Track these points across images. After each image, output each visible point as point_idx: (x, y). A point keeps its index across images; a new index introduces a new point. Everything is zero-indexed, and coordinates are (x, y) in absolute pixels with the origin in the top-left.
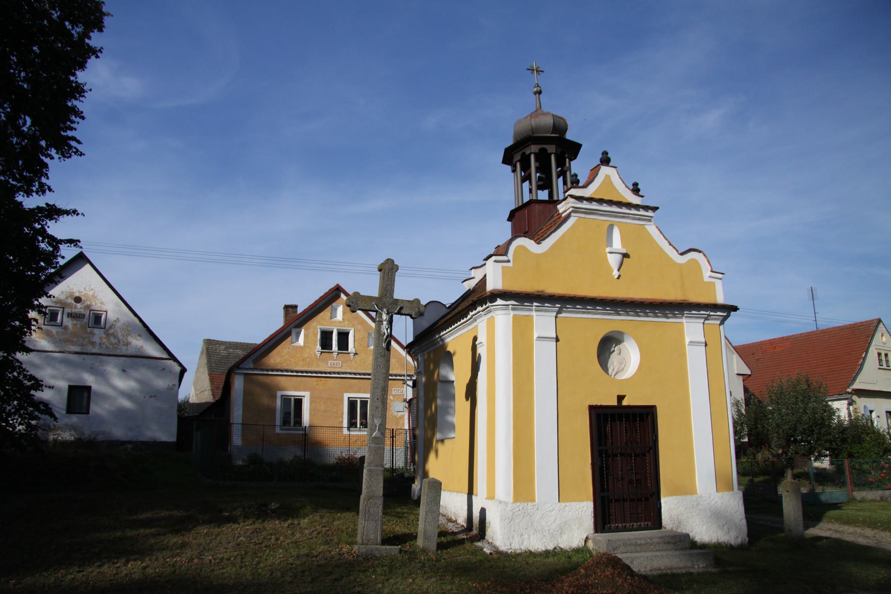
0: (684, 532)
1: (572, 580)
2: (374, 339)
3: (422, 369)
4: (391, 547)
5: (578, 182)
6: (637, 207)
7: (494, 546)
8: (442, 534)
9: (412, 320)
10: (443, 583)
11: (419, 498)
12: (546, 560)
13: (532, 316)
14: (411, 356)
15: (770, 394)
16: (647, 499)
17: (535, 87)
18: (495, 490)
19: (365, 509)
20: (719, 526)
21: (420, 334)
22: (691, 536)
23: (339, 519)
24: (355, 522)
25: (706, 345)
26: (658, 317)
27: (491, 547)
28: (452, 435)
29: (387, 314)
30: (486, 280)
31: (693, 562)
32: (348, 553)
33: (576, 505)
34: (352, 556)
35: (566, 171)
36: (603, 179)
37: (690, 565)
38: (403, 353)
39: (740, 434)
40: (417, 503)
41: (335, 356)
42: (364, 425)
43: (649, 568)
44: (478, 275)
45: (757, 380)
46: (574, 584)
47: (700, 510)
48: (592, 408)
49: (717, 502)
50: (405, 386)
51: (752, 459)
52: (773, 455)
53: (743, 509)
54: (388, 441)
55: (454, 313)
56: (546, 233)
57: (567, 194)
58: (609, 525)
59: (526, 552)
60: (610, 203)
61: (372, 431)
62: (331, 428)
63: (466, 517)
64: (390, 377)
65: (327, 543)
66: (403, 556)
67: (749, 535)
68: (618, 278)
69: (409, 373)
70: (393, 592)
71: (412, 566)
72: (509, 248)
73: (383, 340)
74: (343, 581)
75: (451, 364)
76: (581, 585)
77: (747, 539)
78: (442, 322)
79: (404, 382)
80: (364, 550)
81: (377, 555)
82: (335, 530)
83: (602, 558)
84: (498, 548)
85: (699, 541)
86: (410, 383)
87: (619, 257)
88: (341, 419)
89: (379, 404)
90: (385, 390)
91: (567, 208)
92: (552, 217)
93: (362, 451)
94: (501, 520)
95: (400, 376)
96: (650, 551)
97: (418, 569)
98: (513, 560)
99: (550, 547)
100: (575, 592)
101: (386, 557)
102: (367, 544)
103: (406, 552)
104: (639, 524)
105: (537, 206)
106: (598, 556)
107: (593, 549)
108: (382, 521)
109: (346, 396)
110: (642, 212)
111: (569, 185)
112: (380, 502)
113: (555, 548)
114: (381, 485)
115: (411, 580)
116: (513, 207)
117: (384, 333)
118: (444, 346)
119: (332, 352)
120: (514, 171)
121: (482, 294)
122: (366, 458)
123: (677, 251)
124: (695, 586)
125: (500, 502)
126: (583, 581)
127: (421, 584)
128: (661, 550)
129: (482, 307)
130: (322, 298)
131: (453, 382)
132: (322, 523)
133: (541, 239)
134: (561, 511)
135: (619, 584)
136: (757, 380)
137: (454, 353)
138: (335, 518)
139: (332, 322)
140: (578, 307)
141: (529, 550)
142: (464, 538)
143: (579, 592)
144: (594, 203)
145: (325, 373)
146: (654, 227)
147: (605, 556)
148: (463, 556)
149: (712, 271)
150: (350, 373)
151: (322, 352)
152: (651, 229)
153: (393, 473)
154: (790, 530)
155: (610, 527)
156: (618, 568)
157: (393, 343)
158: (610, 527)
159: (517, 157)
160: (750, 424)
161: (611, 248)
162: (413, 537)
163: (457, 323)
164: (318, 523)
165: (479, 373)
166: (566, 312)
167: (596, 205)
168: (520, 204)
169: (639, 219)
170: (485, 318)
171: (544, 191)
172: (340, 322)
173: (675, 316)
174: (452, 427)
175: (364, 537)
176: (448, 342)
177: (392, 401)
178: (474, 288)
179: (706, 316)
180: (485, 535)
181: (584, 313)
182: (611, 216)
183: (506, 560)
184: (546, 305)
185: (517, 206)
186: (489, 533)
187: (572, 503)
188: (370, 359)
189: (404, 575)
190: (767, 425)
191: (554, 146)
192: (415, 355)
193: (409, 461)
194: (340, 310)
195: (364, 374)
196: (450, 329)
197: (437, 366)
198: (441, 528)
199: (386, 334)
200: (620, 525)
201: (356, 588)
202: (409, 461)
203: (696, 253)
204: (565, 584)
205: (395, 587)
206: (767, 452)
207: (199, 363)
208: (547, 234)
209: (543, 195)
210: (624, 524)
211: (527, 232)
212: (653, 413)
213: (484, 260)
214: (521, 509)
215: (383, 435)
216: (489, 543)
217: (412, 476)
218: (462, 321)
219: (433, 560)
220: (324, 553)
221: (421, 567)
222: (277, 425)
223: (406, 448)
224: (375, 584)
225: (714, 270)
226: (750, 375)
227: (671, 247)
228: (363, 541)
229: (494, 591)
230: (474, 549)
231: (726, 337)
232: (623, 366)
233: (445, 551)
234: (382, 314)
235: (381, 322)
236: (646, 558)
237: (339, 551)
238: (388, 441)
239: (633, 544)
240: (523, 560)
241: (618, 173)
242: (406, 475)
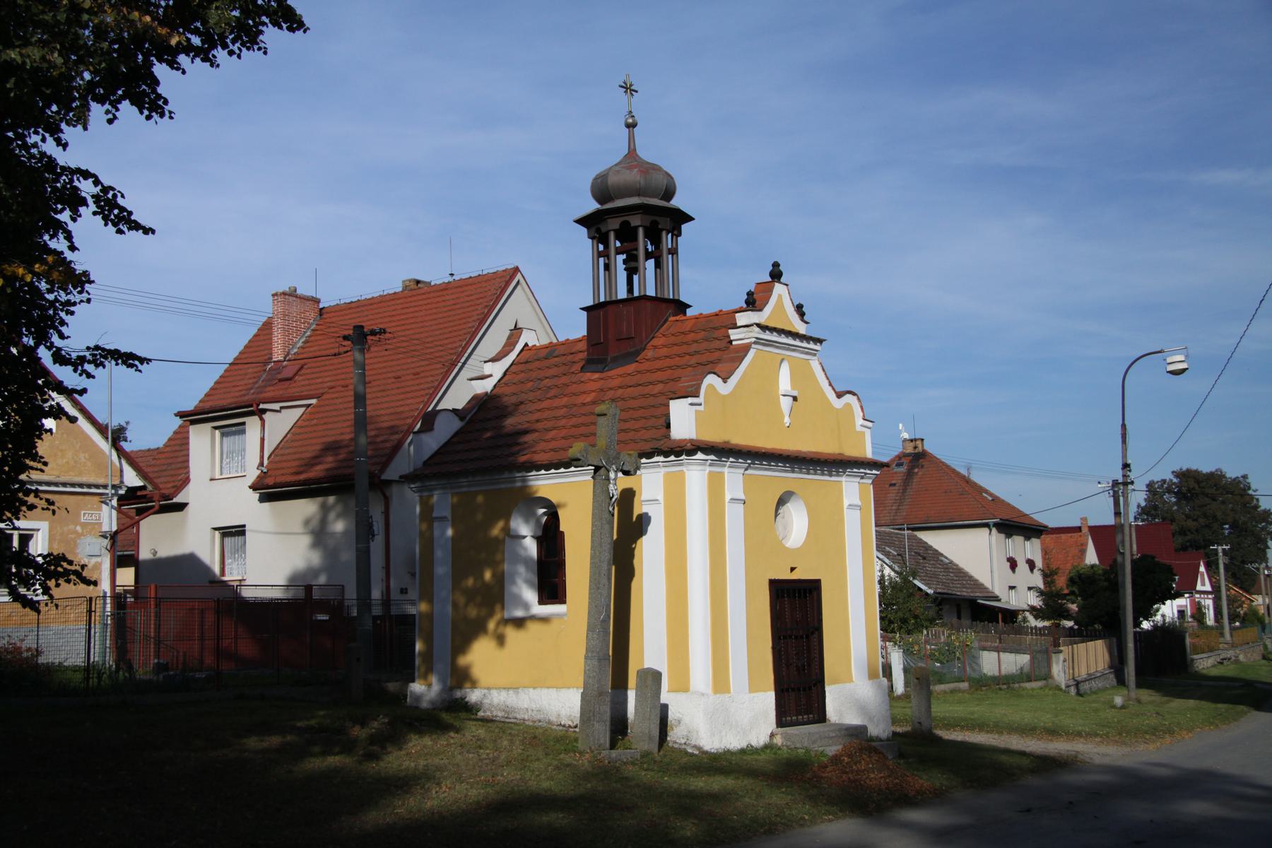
13: (722, 473)
33: (761, 695)
48: (818, 581)
95: (97, 486)
146: (817, 362)
154: (920, 723)
173: (838, 475)
225: (866, 418)
227: (830, 388)
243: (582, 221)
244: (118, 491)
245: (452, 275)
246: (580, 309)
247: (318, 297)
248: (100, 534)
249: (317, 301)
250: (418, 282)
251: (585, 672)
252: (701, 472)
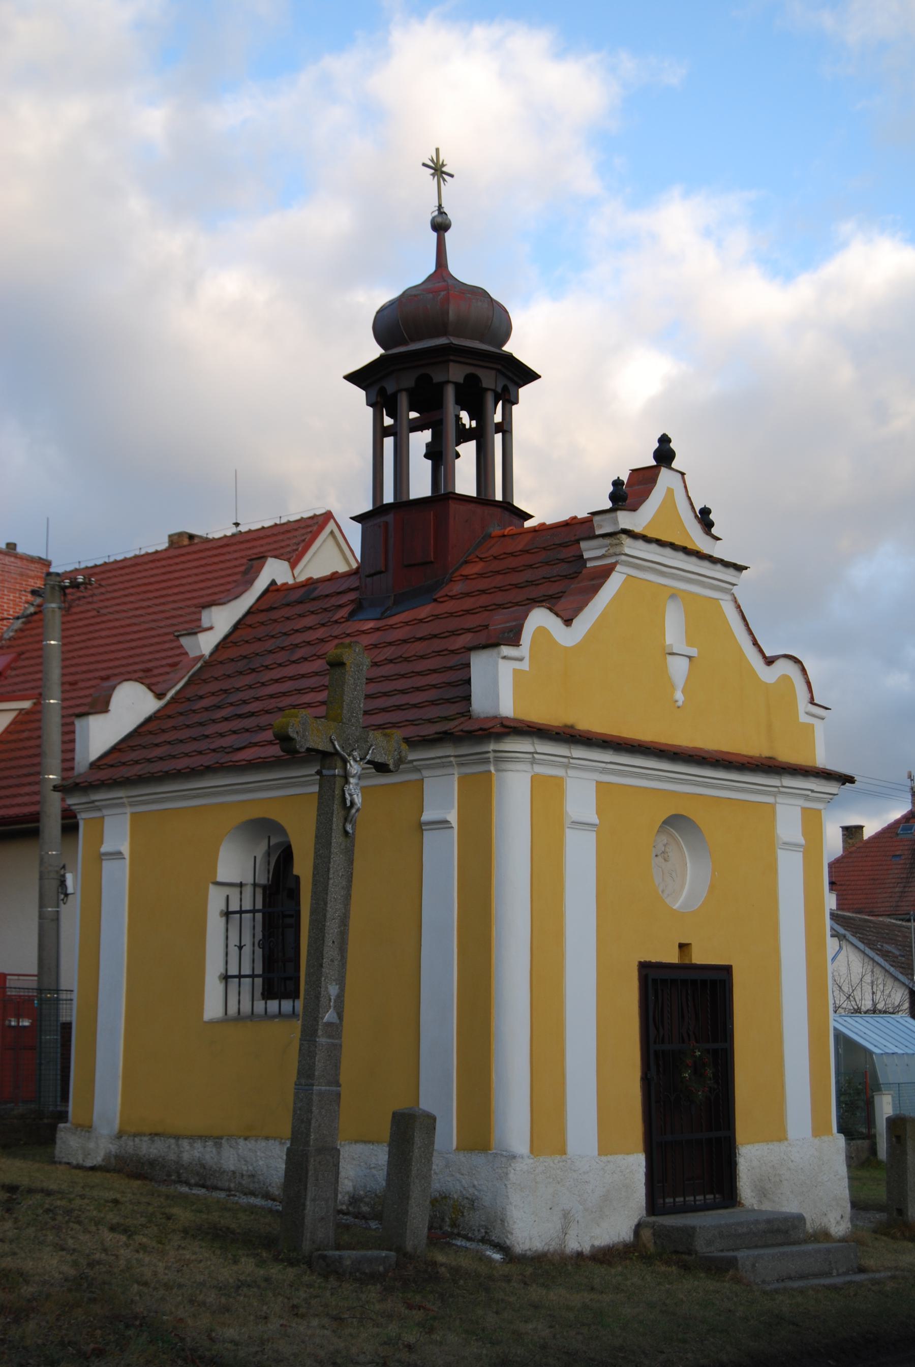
48: (728, 969)
60: (673, 546)
68: (679, 707)
207: (353, 856)
222: (62, 988)
236: (771, 1258)
243: (354, 378)
245: (237, 524)
246: (352, 518)
247: (49, 558)
249: (48, 564)
250: (191, 537)
251: (295, 1111)
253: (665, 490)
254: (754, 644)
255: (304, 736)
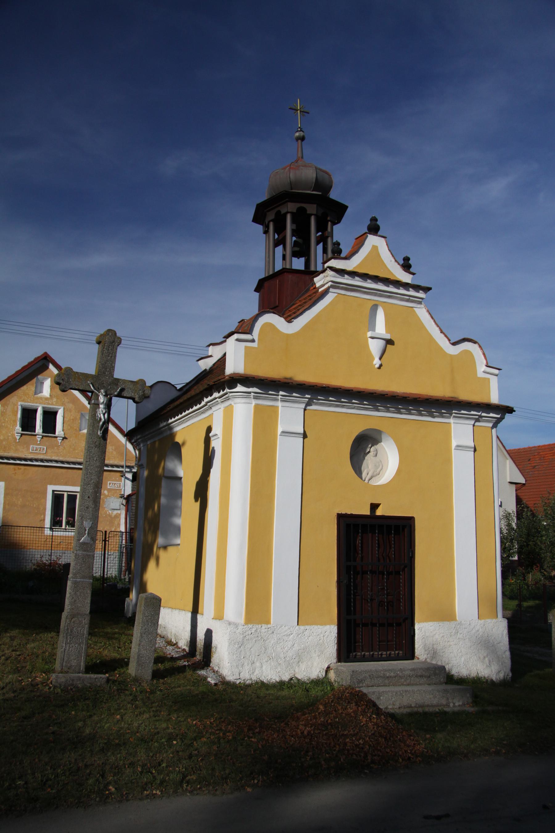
0: (439, 663)
1: (309, 718)
2: (87, 421)
3: (144, 461)
4: (96, 676)
5: (340, 251)
6: (406, 286)
7: (220, 676)
8: (160, 659)
9: (135, 404)
10: (157, 721)
11: (134, 614)
12: (279, 693)
13: (277, 407)
14: (132, 444)
15: (545, 508)
16: (399, 625)
17: (297, 131)
18: (224, 609)
19: (67, 629)
20: (480, 658)
21: (144, 420)
22: (447, 669)
23: (33, 641)
24: (53, 645)
25: (475, 450)
26: (422, 415)
27: (216, 677)
28: (178, 541)
29: (104, 395)
30: (225, 359)
31: (448, 699)
32: (43, 683)
34: (47, 688)
35: (327, 237)
36: (370, 250)
37: (445, 703)
38: (123, 439)
39: (509, 551)
40: (131, 621)
41: (39, 439)
42: (71, 523)
43: (397, 705)
44: (216, 353)
45: (532, 490)
46: (311, 722)
47: (459, 639)
48: (341, 517)
49: (478, 631)
50: (123, 479)
51: (521, 580)
52: (546, 578)
53: (508, 640)
54: (99, 545)
55: (185, 397)
56: (299, 310)
57: (326, 265)
58: (354, 654)
59: (257, 683)
60: (376, 279)
61: (80, 534)
62: (29, 528)
63: (189, 639)
64: (106, 468)
65: (17, 671)
66: (110, 687)
67: (513, 670)
68: (379, 368)
69: (129, 464)
70: (96, 732)
71: (120, 699)
72: (254, 326)
73: (98, 426)
74: (34, 719)
75: (179, 456)
76: (319, 724)
77: (510, 675)
78: (171, 408)
79: (123, 474)
80: (63, 680)
81: (79, 685)
82: (28, 655)
83: (345, 692)
84: (224, 678)
85: (456, 674)
86: (130, 476)
87: (382, 343)
88: (42, 516)
89: (91, 504)
90: (98, 486)
91: (325, 282)
92: (308, 290)
93: (67, 558)
94: (230, 644)
95: (117, 466)
96: (400, 685)
97: (129, 703)
98: (242, 692)
99: (286, 678)
100: (312, 732)
101: (90, 687)
102: (67, 672)
103: (114, 681)
104: (388, 653)
105: (290, 276)
106: (340, 690)
107: (335, 681)
108: (87, 644)
109: (51, 488)
110: (412, 293)
111: (330, 255)
112: (86, 621)
113: (291, 679)
114: (88, 600)
115: (118, 717)
116: (262, 276)
117: (101, 419)
118: (172, 436)
119: (36, 435)
120: (266, 232)
121: (220, 378)
122: (71, 568)
123: (449, 340)
124: (449, 727)
125: (230, 624)
126: (322, 719)
127: (131, 721)
128: (413, 685)
129: (219, 392)
130: (24, 369)
131: (181, 478)
132: (12, 646)
133: (293, 316)
134: (299, 636)
135: (362, 724)
136: (532, 490)
137: (184, 444)
138: (28, 640)
139: (37, 398)
140: (331, 398)
141: (261, 681)
142: (185, 665)
143: (316, 732)
144: (357, 278)
145: (26, 460)
147: (347, 691)
148: (184, 687)
149: (487, 366)
150: (57, 461)
151: (22, 435)
152: (422, 313)
153: (103, 583)
155: (356, 655)
156: (363, 705)
157: (111, 428)
158: (356, 655)
159: (271, 216)
160: (521, 540)
161: (373, 332)
162: (124, 663)
163: (188, 410)
164: (7, 646)
165: (211, 470)
166: (316, 404)
167: (359, 281)
168: (271, 273)
169: (408, 301)
170: (222, 406)
171: (300, 259)
172: (47, 399)
173: (442, 416)
174: (177, 530)
175: (64, 663)
176: (176, 432)
177: (106, 496)
178: (211, 368)
179: (477, 417)
180: (210, 661)
181: (337, 406)
182: (375, 295)
183: (234, 692)
184: (294, 394)
185: (267, 275)
186: (215, 659)
187: (312, 627)
188: (83, 444)
189: (110, 710)
190: (541, 542)
191: (315, 206)
192: (137, 444)
193: (124, 568)
194: (47, 384)
195: (74, 463)
196: (180, 416)
197: (163, 457)
198: (158, 653)
199: (103, 420)
200: (366, 654)
201: (51, 728)
202: (124, 568)
203: (466, 343)
204: (301, 723)
205: (99, 725)
206: (539, 574)
208: (301, 311)
209: (298, 264)
210: (371, 653)
211: (277, 307)
212: (411, 526)
213: (224, 337)
214: (253, 632)
215: (93, 540)
216: (214, 672)
217: (126, 587)
218: (195, 408)
219: (147, 692)
220: (13, 684)
221: (132, 700)
223: (121, 553)
224: (75, 722)
225: (489, 365)
226: (524, 484)
227: (442, 335)
228: (62, 669)
229: (217, 730)
230: (196, 679)
231: (498, 437)
232: (379, 469)
233: (161, 681)
234: (98, 396)
235: (97, 405)
237: (32, 681)
238: (99, 545)
239: (381, 677)
240: (253, 693)
241: (387, 245)
242: (120, 586)
244: (132, 469)
248: (120, 496)
252: (247, 405)
253: (371, 247)
254: (441, 333)
255: (68, 382)
